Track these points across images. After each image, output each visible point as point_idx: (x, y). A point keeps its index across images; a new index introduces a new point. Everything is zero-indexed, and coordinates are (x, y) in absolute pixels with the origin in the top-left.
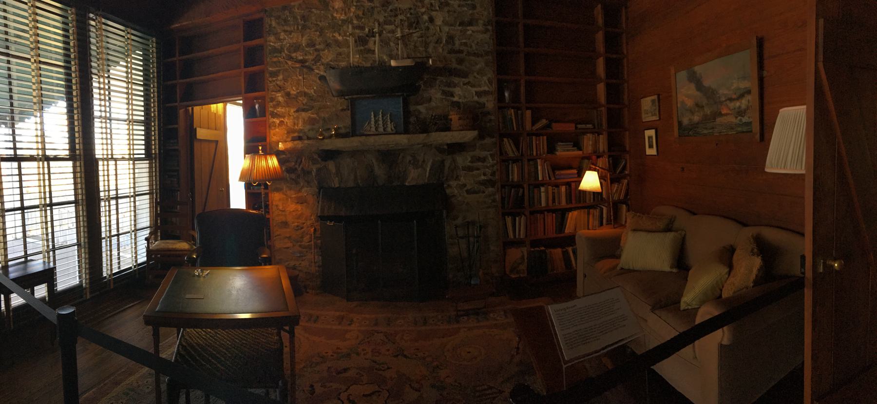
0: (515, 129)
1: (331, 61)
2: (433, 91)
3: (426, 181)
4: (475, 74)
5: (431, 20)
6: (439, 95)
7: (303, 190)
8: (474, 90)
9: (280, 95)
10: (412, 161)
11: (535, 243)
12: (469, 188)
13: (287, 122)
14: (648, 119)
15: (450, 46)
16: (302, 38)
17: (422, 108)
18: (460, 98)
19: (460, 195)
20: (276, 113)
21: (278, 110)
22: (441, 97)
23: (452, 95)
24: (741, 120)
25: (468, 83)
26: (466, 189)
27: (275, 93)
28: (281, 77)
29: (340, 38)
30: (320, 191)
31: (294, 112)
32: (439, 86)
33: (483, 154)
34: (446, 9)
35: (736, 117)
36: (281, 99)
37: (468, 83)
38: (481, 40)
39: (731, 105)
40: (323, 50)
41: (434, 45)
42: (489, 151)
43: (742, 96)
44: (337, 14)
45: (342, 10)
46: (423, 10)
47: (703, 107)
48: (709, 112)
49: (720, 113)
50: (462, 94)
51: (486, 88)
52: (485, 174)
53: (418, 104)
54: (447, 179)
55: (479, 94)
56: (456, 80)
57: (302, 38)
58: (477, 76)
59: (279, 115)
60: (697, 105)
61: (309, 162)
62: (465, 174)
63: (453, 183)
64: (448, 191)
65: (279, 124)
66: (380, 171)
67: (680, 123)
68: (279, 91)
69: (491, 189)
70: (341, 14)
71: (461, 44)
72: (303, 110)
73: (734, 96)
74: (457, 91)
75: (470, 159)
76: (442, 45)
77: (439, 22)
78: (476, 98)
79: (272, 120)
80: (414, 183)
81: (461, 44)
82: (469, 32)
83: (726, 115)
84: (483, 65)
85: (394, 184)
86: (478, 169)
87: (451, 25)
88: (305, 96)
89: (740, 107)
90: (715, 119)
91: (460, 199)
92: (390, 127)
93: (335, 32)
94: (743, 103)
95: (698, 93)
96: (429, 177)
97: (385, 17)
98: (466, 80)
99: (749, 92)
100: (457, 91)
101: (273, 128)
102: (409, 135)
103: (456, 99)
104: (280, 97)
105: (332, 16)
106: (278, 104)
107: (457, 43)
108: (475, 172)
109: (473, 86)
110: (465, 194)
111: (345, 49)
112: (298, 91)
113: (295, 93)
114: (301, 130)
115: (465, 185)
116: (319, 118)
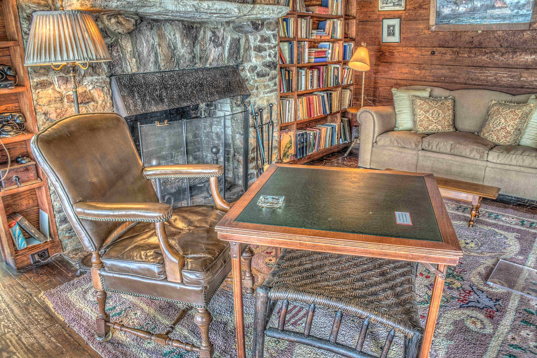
3: (226, 62)
10: (213, 38)
26: (256, 71)
30: (111, 80)
52: (270, 56)
54: (242, 61)
64: (242, 74)
67: (438, 14)
75: (259, 38)
80: (215, 65)
96: (228, 58)
102: (239, 5)
110: (256, 78)
115: (256, 67)
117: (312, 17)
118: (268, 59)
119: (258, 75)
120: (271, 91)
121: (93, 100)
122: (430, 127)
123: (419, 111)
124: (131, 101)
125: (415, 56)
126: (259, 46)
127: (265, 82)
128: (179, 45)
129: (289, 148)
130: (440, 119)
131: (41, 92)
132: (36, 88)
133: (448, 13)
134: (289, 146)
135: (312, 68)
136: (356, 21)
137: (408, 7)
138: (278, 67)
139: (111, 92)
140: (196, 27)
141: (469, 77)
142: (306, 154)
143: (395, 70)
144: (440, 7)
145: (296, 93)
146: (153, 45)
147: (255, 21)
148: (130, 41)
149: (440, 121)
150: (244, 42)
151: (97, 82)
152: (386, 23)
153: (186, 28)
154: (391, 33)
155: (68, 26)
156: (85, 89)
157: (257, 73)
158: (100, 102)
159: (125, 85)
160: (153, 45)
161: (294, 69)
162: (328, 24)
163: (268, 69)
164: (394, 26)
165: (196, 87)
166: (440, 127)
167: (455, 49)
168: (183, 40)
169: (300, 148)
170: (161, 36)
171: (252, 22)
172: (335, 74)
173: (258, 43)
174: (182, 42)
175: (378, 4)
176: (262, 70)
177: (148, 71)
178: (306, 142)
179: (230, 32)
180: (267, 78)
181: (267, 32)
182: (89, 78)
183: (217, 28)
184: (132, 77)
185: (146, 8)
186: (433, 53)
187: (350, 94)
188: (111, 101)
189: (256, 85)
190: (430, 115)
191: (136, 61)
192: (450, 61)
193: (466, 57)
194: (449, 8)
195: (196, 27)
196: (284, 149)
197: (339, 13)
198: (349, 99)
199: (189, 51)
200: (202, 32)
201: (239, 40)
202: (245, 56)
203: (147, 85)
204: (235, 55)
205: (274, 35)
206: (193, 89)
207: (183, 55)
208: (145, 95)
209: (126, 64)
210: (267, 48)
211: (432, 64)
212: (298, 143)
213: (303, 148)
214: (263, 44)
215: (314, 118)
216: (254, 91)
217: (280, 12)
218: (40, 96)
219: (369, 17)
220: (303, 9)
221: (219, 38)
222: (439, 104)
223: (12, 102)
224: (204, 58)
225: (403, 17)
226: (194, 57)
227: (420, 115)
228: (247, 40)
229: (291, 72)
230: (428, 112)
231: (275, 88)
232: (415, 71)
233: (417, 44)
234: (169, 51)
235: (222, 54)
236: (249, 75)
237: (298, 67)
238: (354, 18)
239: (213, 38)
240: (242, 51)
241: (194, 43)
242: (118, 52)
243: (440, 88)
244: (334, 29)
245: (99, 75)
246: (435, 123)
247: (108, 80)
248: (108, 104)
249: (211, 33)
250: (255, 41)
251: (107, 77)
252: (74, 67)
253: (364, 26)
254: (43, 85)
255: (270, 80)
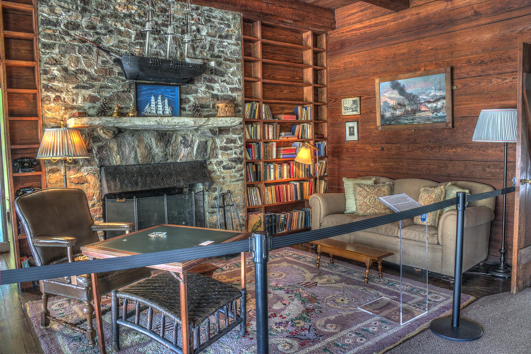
0: (256, 118)
1: (113, 46)
2: (199, 85)
3: (194, 158)
4: (229, 75)
5: (198, 30)
6: (203, 89)
7: (83, 170)
8: (228, 86)
9: (56, 68)
10: (183, 141)
11: (267, 209)
12: (225, 164)
13: (64, 99)
14: (347, 114)
15: (211, 52)
16: (82, 18)
17: (191, 98)
18: (218, 92)
19: (219, 170)
20: (52, 88)
21: (53, 84)
22: (205, 89)
23: (213, 90)
24: (436, 115)
25: (224, 81)
26: (222, 165)
27: (50, 66)
28: (57, 51)
29: (122, 29)
30: (101, 169)
31: (73, 88)
32: (204, 81)
33: (235, 136)
34: (209, 24)
35: (433, 113)
36: (56, 73)
37: (224, 81)
38: (234, 50)
39: (429, 105)
40: (105, 35)
41: (200, 49)
42: (238, 135)
43: (437, 100)
44: (119, 7)
45: (125, 5)
46: (193, 22)
47: (404, 106)
48: (410, 109)
49: (420, 110)
50: (220, 89)
51: (237, 86)
52: (235, 153)
53: (187, 93)
54: (209, 157)
55: (232, 90)
56: (216, 78)
57: (82, 18)
58: (231, 77)
59: (54, 89)
60: (399, 104)
61: (89, 141)
62: (222, 152)
63: (214, 161)
64: (209, 167)
65: (54, 100)
66: (157, 150)
67: (382, 117)
68: (55, 64)
69: (239, 165)
70: (124, 8)
71: (219, 51)
72: (84, 88)
73: (431, 100)
74: (216, 86)
75: (225, 141)
76: (206, 50)
77: (204, 33)
78: (230, 93)
79: (45, 94)
80: (184, 160)
81: (219, 51)
82: (226, 44)
83: (425, 111)
84: (235, 68)
85: (169, 161)
86: (231, 149)
87: (214, 37)
88: (85, 75)
89: (436, 107)
90: (415, 113)
91: (218, 173)
92: (168, 110)
93: (117, 22)
94: (439, 104)
95: (402, 97)
96: (196, 155)
97: (163, 20)
98: (223, 79)
99: (444, 98)
100: (216, 86)
101: (47, 102)
102: (195, 118)
103: (215, 92)
104: (55, 71)
105: (114, 8)
106: (54, 78)
107: (216, 50)
108: (229, 152)
109: (228, 83)
110: (222, 170)
111: (126, 39)
112: (77, 68)
113: (73, 69)
114: (81, 107)
115: (222, 162)
116: (100, 96)
117: (279, 123)
118: (234, 156)
119: (224, 168)
120: (237, 181)
121: (87, 182)
122: (368, 211)
123: (359, 197)
124: (112, 184)
125: (370, 151)
126: (225, 146)
127: (231, 173)
128: (154, 146)
129: (258, 226)
130: (376, 204)
131: (51, 176)
132: (49, 173)
133: (389, 116)
134: (258, 225)
135: (281, 163)
136: (328, 124)
137: (362, 112)
138: (244, 161)
139: (100, 177)
140: (169, 134)
141: (409, 168)
142: (275, 232)
143: (356, 163)
144: (383, 111)
145: (264, 183)
146: (134, 146)
147: (212, 129)
148: (116, 144)
149: (376, 205)
150: (211, 143)
151: (90, 170)
152: (349, 125)
153: (159, 135)
154: (352, 134)
155: (60, 137)
156: (82, 175)
157: (222, 166)
158: (92, 184)
159: (110, 173)
160: (134, 146)
161: (261, 163)
162: (298, 128)
163: (234, 164)
164: (353, 128)
165: (166, 176)
166: (377, 211)
167: (397, 145)
168: (157, 143)
169: (268, 227)
170: (140, 141)
171: (210, 130)
172: (306, 167)
173: (225, 145)
174: (157, 144)
175: (341, 110)
176: (228, 164)
177: (129, 164)
178: (275, 222)
179: (198, 137)
180: (234, 170)
181: (233, 136)
182: (86, 168)
183: (187, 134)
184: (116, 168)
185: (121, 124)
186: (383, 149)
187: (325, 184)
188: (100, 183)
189: (222, 175)
190: (368, 201)
191: (120, 157)
192: (395, 154)
193: (406, 152)
194: (390, 112)
195: (169, 134)
196: (252, 227)
197: (309, 119)
198: (324, 189)
199: (162, 150)
200: (174, 137)
201: (206, 142)
202: (211, 154)
203: (127, 173)
204: (203, 153)
205: (240, 138)
206: (163, 177)
207: (157, 154)
208: (124, 180)
209: (113, 159)
210: (233, 148)
211: (382, 158)
212: (266, 222)
213: (271, 227)
214: (229, 145)
215: (283, 203)
216: (221, 180)
217: (233, 122)
218: (51, 177)
219: (336, 121)
220: (269, 117)
221: (188, 141)
222: (376, 190)
223: (36, 181)
224: (175, 154)
225: (360, 120)
226: (166, 155)
227: (359, 200)
228: (214, 142)
229: (259, 166)
230: (366, 197)
231: (241, 178)
232: (371, 164)
233: (371, 142)
234: (146, 150)
235: (190, 153)
236: (215, 168)
237: (265, 162)
238: (326, 122)
239: (183, 141)
240: (209, 150)
241: (166, 145)
242: (107, 151)
243: (427, 180)
244: (304, 130)
245: (92, 166)
246: (373, 207)
247: (99, 169)
248: (98, 185)
249: (181, 137)
250: (221, 143)
251: (98, 167)
252: (65, 161)
253: (334, 128)
254: (53, 171)
255: (236, 172)
